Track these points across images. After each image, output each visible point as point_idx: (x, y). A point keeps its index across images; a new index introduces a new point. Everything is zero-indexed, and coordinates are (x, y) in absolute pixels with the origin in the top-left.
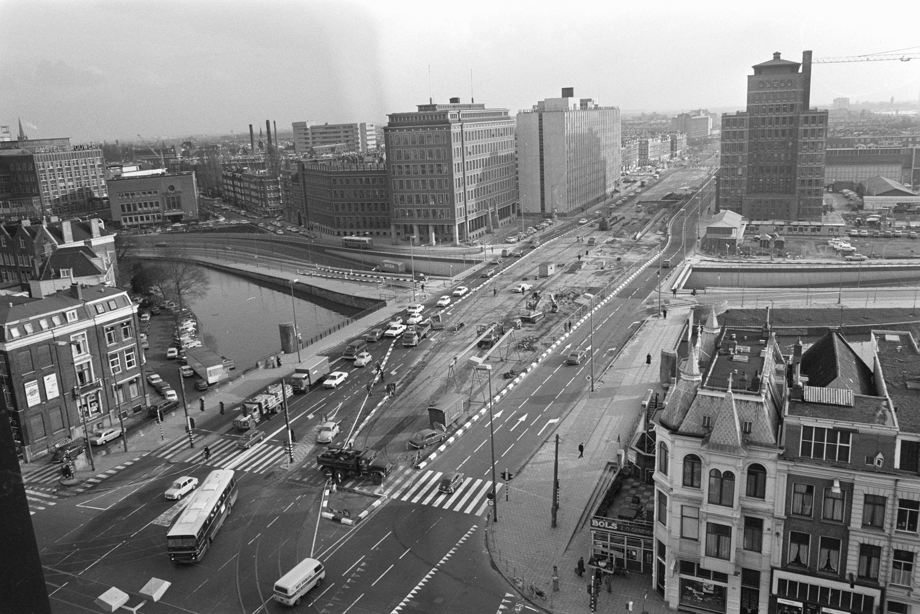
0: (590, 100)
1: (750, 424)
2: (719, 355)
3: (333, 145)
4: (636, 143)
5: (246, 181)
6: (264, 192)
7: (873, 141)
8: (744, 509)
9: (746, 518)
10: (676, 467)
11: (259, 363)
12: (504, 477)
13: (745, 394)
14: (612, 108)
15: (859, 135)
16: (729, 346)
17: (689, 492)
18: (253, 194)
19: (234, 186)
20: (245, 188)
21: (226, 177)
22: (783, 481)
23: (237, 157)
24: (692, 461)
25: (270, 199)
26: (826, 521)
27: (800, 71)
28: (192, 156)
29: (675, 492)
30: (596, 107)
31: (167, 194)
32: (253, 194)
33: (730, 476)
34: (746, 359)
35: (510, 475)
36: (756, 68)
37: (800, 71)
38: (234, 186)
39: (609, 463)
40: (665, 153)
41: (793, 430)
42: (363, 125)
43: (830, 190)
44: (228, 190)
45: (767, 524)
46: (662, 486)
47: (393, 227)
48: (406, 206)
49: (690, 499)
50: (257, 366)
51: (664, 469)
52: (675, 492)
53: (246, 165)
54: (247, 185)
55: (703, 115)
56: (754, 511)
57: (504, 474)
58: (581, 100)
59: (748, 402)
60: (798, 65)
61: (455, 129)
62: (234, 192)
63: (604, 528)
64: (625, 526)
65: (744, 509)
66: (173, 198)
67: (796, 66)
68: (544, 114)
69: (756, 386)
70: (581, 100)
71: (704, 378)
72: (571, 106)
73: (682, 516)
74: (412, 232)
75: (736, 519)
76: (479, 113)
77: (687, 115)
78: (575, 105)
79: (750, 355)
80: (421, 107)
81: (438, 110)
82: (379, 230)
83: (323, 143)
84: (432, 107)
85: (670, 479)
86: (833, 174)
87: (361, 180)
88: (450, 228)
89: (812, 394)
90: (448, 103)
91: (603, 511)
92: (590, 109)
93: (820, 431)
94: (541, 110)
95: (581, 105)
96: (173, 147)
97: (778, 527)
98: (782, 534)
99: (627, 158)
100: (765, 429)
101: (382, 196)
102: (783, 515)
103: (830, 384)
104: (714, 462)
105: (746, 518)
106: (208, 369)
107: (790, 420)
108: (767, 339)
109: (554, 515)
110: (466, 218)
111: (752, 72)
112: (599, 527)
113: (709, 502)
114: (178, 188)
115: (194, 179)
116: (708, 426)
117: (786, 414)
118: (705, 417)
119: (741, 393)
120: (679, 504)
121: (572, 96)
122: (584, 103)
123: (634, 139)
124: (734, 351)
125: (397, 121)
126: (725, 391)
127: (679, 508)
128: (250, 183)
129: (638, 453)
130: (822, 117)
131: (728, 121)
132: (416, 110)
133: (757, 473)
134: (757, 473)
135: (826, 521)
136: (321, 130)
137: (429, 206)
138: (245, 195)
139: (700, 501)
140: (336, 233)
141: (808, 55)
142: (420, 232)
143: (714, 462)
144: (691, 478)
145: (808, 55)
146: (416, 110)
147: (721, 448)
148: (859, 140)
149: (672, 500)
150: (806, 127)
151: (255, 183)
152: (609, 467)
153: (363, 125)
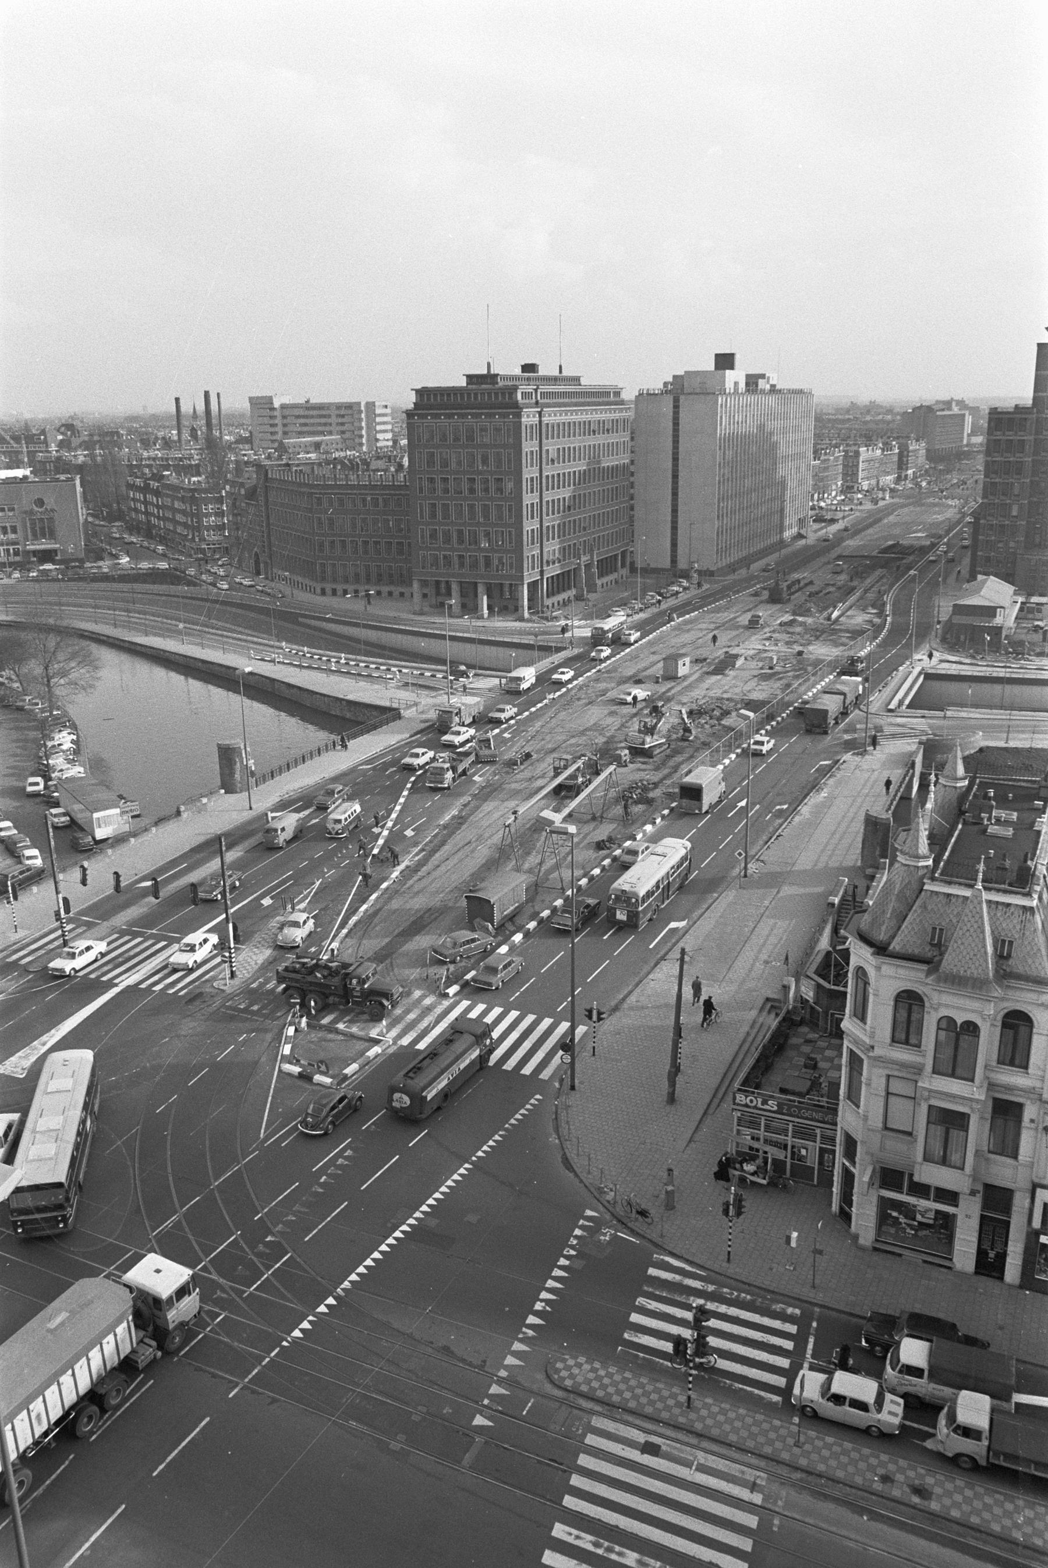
0: (763, 376)
3: (317, 439)
4: (839, 453)
5: (168, 496)
9: (995, 1100)
11: (182, 808)
13: (1005, 892)
14: (801, 392)
18: (179, 517)
19: (146, 503)
20: (163, 507)
23: (152, 454)
24: (909, 1002)
29: (878, 1052)
30: (773, 390)
32: (179, 517)
33: (971, 1029)
35: (599, 1013)
38: (146, 503)
39: (768, 999)
40: (888, 473)
42: (371, 406)
44: (136, 510)
46: (856, 1042)
47: (416, 585)
48: (439, 549)
50: (178, 813)
51: (861, 1015)
52: (878, 1052)
53: (167, 467)
54: (168, 501)
55: (956, 410)
56: (1009, 1088)
57: (590, 1011)
58: (748, 376)
59: (1008, 905)
62: (147, 513)
63: (755, 1107)
65: (992, 1086)
66: (42, 520)
70: (748, 376)
71: (936, 862)
72: (729, 386)
73: (888, 1093)
77: (929, 409)
78: (736, 384)
79: (1016, 826)
80: (470, 378)
82: (392, 588)
84: (490, 378)
85: (869, 1029)
87: (364, 500)
90: (518, 371)
92: (763, 392)
106: (96, 815)
110: (542, 573)
112: (746, 1106)
113: (934, 1072)
114: (50, 502)
115: (79, 489)
118: (934, 929)
122: (752, 381)
123: (837, 446)
124: (989, 819)
125: (430, 401)
128: (174, 498)
132: (463, 382)
136: (297, 412)
138: (165, 519)
139: (919, 1070)
140: (318, 591)
142: (463, 595)
143: (947, 1004)
144: (906, 1031)
146: (463, 382)
152: (769, 1005)
153: (371, 406)
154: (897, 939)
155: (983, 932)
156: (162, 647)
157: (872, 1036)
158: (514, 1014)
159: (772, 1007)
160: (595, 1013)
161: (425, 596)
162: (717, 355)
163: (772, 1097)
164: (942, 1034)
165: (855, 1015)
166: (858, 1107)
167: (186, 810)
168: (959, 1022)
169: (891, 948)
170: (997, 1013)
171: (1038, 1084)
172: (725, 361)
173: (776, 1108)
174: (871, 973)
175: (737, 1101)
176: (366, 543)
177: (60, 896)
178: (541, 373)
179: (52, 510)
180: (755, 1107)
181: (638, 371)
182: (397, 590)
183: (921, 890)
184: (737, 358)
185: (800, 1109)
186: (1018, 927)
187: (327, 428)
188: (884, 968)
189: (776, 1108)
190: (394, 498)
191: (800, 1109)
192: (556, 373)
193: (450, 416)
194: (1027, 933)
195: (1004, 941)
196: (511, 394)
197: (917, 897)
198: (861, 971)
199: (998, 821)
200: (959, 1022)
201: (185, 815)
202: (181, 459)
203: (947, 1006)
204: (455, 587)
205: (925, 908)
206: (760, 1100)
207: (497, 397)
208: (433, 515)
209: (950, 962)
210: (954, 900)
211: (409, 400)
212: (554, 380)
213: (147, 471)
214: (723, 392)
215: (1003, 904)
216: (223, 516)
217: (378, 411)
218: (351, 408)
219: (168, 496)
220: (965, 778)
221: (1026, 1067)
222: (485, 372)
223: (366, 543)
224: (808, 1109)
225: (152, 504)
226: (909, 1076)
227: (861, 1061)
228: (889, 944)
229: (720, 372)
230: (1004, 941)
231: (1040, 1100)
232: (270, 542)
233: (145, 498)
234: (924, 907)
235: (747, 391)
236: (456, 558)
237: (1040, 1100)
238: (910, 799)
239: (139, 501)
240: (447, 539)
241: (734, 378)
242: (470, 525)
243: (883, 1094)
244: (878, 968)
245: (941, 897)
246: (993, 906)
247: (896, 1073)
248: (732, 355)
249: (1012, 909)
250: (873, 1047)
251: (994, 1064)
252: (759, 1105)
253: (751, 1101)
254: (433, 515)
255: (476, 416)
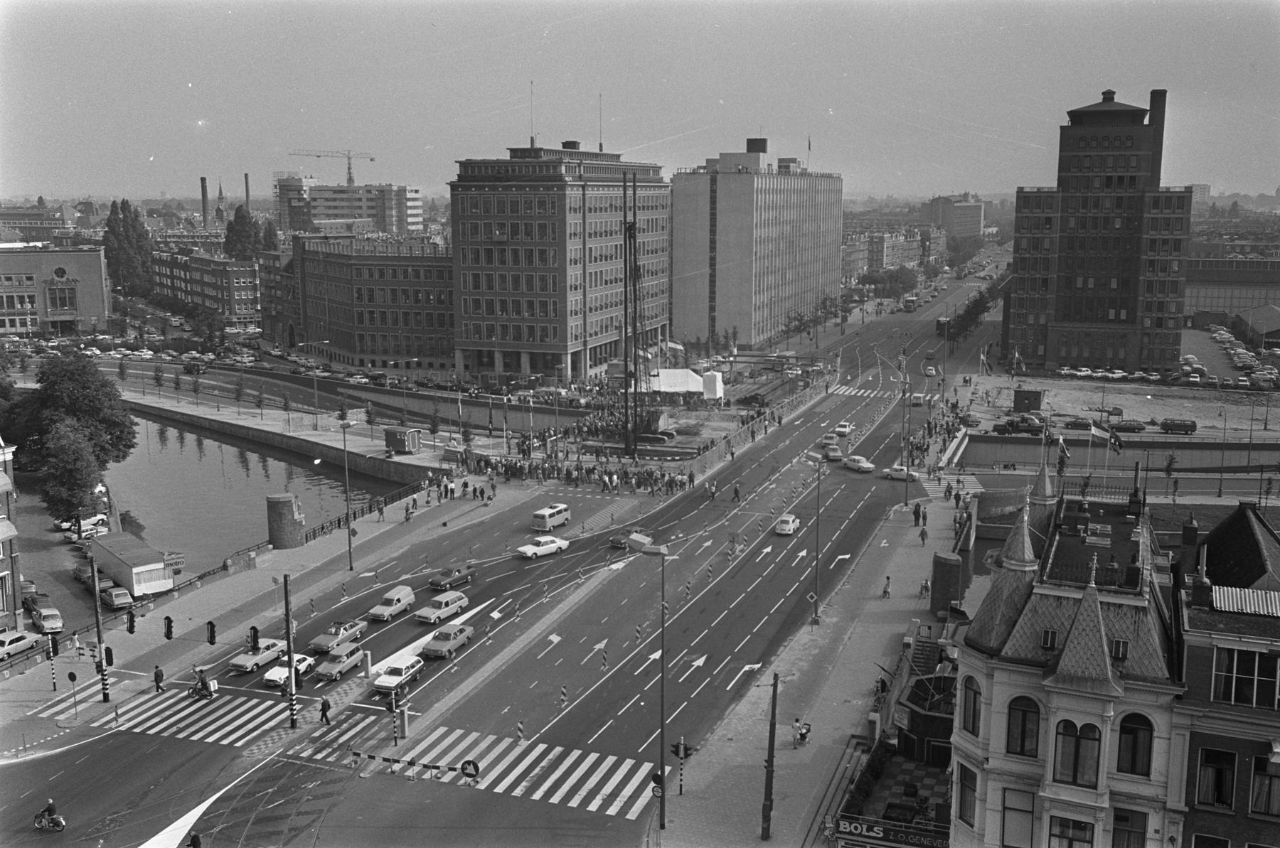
0: (794, 161)
1: (1125, 644)
2: (1061, 534)
3: (350, 221)
4: (865, 238)
5: (197, 270)
6: (228, 289)
7: (1254, 249)
8: (1113, 794)
9: (1115, 809)
10: (995, 725)
11: (229, 562)
12: (676, 753)
13: (1116, 592)
14: (830, 176)
15: (1232, 240)
16: (1077, 521)
17: (1016, 765)
18: (208, 291)
19: (172, 277)
20: (192, 281)
21: (161, 262)
22: (1181, 746)
23: (177, 232)
24: (1024, 713)
25: (240, 302)
26: (1257, 817)
27: (1146, 121)
28: (94, 227)
29: (992, 764)
30: (804, 174)
31: (52, 282)
32: (208, 291)
33: (1090, 732)
34: (1107, 542)
35: (686, 749)
36: (1072, 114)
37: (1146, 121)
38: (172, 277)
39: (853, 736)
40: (911, 259)
41: (1202, 655)
42: (402, 191)
43: (1189, 324)
44: (162, 285)
45: (1154, 822)
46: (967, 756)
47: (458, 355)
48: (483, 319)
49: (1020, 777)
50: (225, 567)
51: (972, 728)
52: (992, 764)
53: (195, 244)
54: (197, 276)
55: (972, 202)
56: (1132, 797)
57: (677, 747)
58: (780, 160)
59: (1120, 606)
60: (1143, 112)
61: (573, 194)
62: (173, 288)
63: (860, 835)
64: (896, 832)
65: (1113, 794)
66: (62, 290)
67: (1141, 113)
68: (719, 177)
69: (1132, 580)
70: (780, 160)
71: (1043, 567)
72: (763, 166)
73: (1005, 808)
74: (491, 364)
75: (1102, 809)
76: (605, 167)
77: (947, 200)
78: (769, 165)
79: (1115, 536)
80: (514, 152)
81: (544, 158)
82: (432, 360)
83: (328, 216)
84: (534, 152)
85: (982, 742)
86: (1196, 299)
87: (406, 271)
88: (558, 359)
89: (1225, 598)
90: (560, 148)
91: (854, 807)
92: (795, 174)
93: (1246, 657)
94: (714, 171)
95: (780, 167)
96: (60, 209)
97: (1173, 828)
98: (1180, 840)
99: (849, 264)
100: (1149, 651)
101: (440, 302)
102: (1182, 806)
103: (1256, 584)
104: (1063, 707)
105: (1115, 809)
106: (135, 570)
107: (1192, 638)
108: (1137, 515)
109: (766, 818)
110: (585, 343)
111: (1066, 121)
112: (850, 833)
113: (1055, 780)
114: (72, 272)
115: (103, 260)
116: (1052, 648)
117: (1187, 628)
118: (1047, 632)
119: (1109, 591)
120: (1000, 785)
121: (764, 151)
122: (785, 165)
123: (862, 233)
124: (1085, 531)
125: (473, 176)
126: (1084, 588)
127: (1000, 793)
128: (203, 272)
129: (912, 710)
130: (1183, 198)
131: (1025, 199)
132: (506, 156)
133: (1135, 730)
134: (1135, 730)
135: (1257, 817)
136: (327, 195)
137: (523, 319)
138: (192, 293)
139: (1037, 782)
140: (357, 362)
141: (1158, 98)
142: (507, 366)
143: (1063, 707)
144: (1022, 737)
145: (1158, 98)
146: (506, 156)
147: (1078, 683)
148: (1233, 247)
149: (985, 781)
150: (1155, 213)
151: (213, 273)
152: (854, 741)
153: (402, 191)
154: (1007, 647)
155: (1099, 631)
156: (194, 413)
157: (986, 747)
158: (593, 757)
159: (858, 744)
160: (682, 747)
161: (466, 367)
162: (749, 141)
163: (877, 822)
164: (1060, 737)
165: (965, 728)
166: (972, 826)
167: (234, 564)
168: (1079, 726)
169: (1003, 653)
170: (1116, 717)
171: (1160, 792)
172: (757, 146)
173: (881, 835)
174: (981, 681)
175: (841, 829)
176: (406, 314)
177: (103, 646)
178: (581, 149)
179: (75, 281)
180: (860, 835)
181: (671, 153)
182: (437, 362)
183: (1030, 594)
184: (769, 143)
185: (907, 834)
186: (1132, 628)
187: (359, 211)
188: (997, 674)
189: (881, 835)
190: (437, 269)
191: (907, 834)
192: (597, 151)
193: (494, 188)
194: (1142, 634)
195: (1118, 642)
196: (555, 168)
197: (1026, 602)
198: (969, 680)
199: (1094, 534)
200: (1079, 726)
201: (231, 570)
202: (207, 237)
203: (1067, 710)
204: (498, 358)
205: (1036, 611)
206: (865, 827)
207: (541, 171)
208: (477, 286)
209: (1067, 663)
210: (1064, 602)
211: (453, 174)
212: (595, 155)
213: (173, 245)
214: (757, 173)
215: (1114, 604)
216: (256, 290)
217: (409, 195)
218: (383, 192)
219: (197, 270)
220: (1054, 496)
221: (1147, 774)
222: (529, 146)
223: (406, 314)
224: (915, 835)
225: (180, 278)
226: (1026, 788)
227: (974, 776)
228: (1000, 650)
229: (753, 155)
230: (1118, 642)
231: (1165, 808)
232: (305, 312)
233: (172, 272)
234: (1035, 611)
235: (779, 173)
236: (499, 328)
237: (1165, 808)
238: (968, 551)
239: (166, 275)
240: (491, 310)
241: (768, 160)
242: (513, 295)
243: (1000, 808)
244: (990, 676)
245: (1051, 600)
246: (1105, 607)
247: (1012, 786)
248: (764, 141)
249: (1125, 609)
250: (987, 759)
251: (1115, 771)
252: (865, 833)
253: (856, 828)
254: (477, 286)
255: (520, 188)
